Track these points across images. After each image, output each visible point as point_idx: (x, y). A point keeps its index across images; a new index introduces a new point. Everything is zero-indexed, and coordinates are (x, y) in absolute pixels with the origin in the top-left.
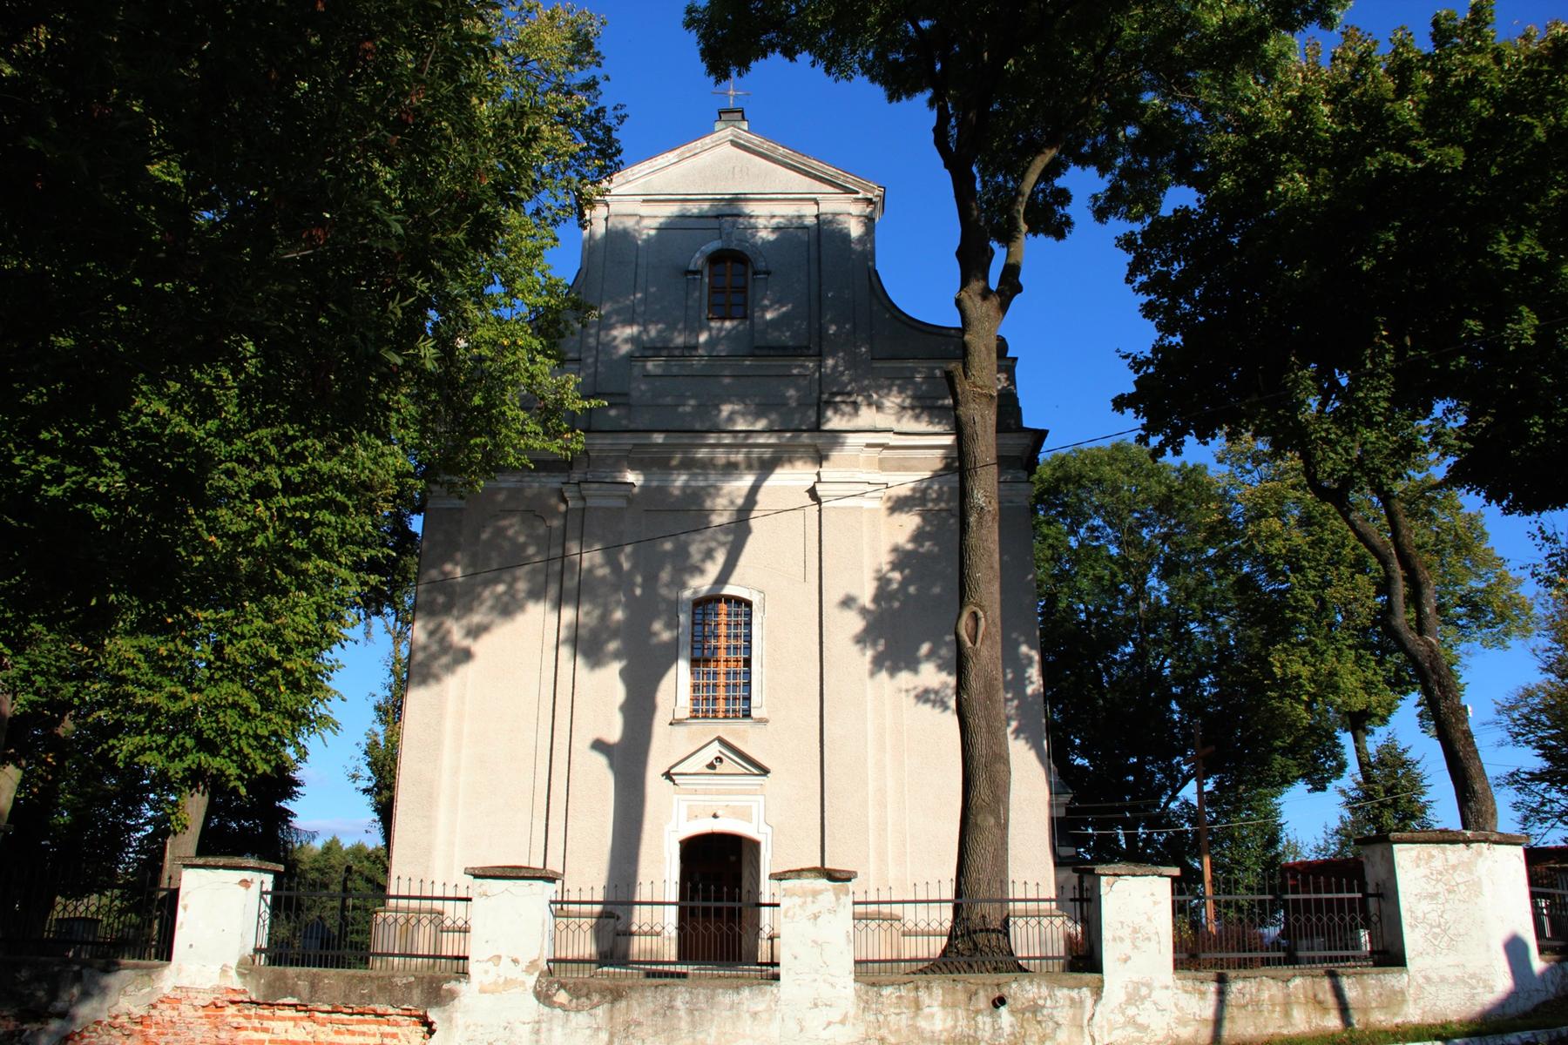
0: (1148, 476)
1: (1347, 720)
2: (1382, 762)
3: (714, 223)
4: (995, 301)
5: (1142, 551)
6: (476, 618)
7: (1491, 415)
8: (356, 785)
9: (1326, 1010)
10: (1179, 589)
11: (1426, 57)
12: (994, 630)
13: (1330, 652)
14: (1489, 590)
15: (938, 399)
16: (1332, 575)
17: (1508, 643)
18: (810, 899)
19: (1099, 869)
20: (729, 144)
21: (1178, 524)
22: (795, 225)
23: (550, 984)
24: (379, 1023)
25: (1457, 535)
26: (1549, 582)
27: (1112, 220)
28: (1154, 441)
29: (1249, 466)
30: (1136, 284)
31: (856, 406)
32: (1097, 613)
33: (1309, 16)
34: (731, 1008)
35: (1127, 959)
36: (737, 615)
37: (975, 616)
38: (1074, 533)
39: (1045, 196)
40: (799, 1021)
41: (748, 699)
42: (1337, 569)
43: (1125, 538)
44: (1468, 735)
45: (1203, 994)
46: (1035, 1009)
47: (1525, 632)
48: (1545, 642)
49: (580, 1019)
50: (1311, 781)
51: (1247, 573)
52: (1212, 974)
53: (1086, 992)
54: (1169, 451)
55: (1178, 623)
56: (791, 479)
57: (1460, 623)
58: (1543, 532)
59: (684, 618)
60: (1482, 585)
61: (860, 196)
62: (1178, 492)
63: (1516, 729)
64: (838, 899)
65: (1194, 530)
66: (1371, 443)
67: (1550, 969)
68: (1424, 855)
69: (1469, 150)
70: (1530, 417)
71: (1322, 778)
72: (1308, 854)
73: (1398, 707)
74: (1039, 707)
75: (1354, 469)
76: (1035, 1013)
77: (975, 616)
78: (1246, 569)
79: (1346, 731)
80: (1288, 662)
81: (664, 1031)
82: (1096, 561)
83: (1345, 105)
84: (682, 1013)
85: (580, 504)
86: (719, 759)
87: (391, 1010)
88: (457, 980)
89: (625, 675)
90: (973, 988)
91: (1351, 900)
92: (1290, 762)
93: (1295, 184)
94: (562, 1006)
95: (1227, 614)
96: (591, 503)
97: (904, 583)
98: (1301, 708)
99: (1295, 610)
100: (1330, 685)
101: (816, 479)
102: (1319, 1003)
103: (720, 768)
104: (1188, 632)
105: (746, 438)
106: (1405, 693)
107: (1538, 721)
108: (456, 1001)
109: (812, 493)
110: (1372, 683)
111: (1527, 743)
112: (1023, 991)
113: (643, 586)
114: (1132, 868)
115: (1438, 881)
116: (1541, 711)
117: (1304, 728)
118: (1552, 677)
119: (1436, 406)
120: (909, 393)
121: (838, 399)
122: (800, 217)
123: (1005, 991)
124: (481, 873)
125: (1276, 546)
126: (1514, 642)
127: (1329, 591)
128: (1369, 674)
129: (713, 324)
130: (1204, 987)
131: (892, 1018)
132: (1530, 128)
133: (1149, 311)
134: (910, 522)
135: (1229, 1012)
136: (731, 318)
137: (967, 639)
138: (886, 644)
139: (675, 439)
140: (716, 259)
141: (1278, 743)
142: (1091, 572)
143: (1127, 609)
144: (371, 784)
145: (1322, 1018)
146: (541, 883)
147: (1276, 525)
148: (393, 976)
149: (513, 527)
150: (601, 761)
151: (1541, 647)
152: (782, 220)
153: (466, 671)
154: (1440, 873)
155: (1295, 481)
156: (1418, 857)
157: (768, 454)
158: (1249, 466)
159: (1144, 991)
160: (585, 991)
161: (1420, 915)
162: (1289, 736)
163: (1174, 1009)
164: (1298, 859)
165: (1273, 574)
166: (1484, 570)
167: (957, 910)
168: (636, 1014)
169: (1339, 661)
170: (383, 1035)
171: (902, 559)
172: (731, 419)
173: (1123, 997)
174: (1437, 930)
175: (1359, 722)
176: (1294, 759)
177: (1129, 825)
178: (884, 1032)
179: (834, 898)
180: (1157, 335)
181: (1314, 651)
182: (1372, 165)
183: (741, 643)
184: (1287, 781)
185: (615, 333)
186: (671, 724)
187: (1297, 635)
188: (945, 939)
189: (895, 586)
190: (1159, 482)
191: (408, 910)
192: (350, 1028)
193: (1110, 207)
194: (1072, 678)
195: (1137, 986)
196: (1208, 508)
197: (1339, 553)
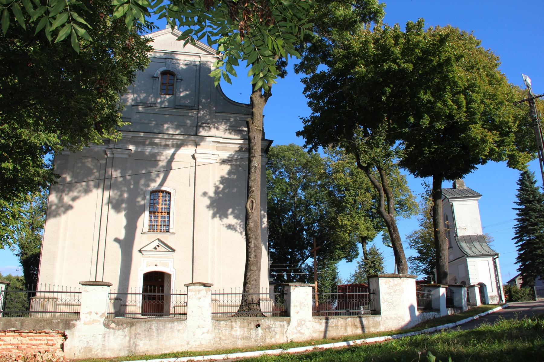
0: (300, 156)
1: (360, 239)
2: (371, 253)
3: (164, 61)
4: (264, 98)
5: (297, 181)
6: (75, 194)
7: (414, 147)
8: (13, 253)
9: (357, 328)
10: (308, 194)
11: (404, 34)
12: (258, 207)
13: (357, 217)
14: (406, 200)
15: (238, 127)
16: (359, 192)
17: (411, 217)
18: (198, 292)
19: (290, 284)
20: (170, 33)
21: (309, 173)
22: (193, 64)
23: (109, 321)
24: (47, 336)
25: (398, 182)
26: (426, 199)
27: (300, 73)
28: (309, 147)
29: (334, 155)
30: (306, 95)
31: (210, 128)
32: (280, 201)
33: (371, 19)
34: (171, 328)
35: (298, 312)
36: (165, 197)
37: (252, 202)
38: (274, 173)
39: (279, 63)
40: (193, 333)
41: (168, 226)
42: (360, 190)
43: (291, 176)
44: (401, 245)
45: (321, 323)
46: (269, 328)
47: (416, 213)
48: (421, 217)
49: (120, 333)
50: (348, 259)
51: (331, 191)
52: (324, 317)
53: (285, 323)
54: (313, 151)
55: (307, 205)
56: (186, 151)
57: (397, 210)
58: (425, 184)
59: (148, 197)
60: (404, 198)
61: (215, 56)
62: (310, 162)
63: (411, 244)
64: (207, 293)
65: (314, 175)
66: (378, 153)
67: (420, 315)
68: (388, 281)
69: (414, 65)
70: (424, 148)
71: (351, 258)
72: (344, 283)
73: (377, 235)
74: (266, 231)
75: (372, 161)
76: (269, 329)
77: (252, 202)
78: (331, 189)
79: (359, 243)
80: (343, 220)
81: (148, 336)
82: (281, 183)
83: (378, 45)
84: (154, 330)
85: (112, 156)
86: (158, 246)
87: (51, 331)
88: (76, 320)
89: (126, 216)
90: (250, 321)
91: (366, 295)
92: (341, 252)
93: (361, 69)
94: (113, 329)
95: (323, 203)
96: (116, 155)
97: (223, 189)
98: (347, 235)
99: (346, 203)
100: (356, 227)
101: (195, 152)
102: (355, 326)
103: (158, 249)
104: (310, 209)
105: (172, 136)
106: (379, 231)
107: (418, 241)
108: (75, 327)
109: (193, 157)
110: (369, 228)
111: (414, 248)
112: (266, 322)
113: (134, 185)
114: (300, 284)
115: (391, 289)
116: (419, 238)
117: (347, 241)
118: (423, 227)
119: (396, 142)
120: (228, 124)
121: (204, 125)
122: (195, 61)
123: (260, 322)
124: (85, 283)
125: (341, 182)
126: (412, 216)
127: (357, 198)
128: (368, 225)
129: (162, 96)
130: (321, 321)
131: (224, 331)
132: (432, 60)
133: (310, 104)
134: (226, 168)
135: (329, 328)
136: (168, 94)
137: (249, 209)
138: (217, 210)
139: (147, 135)
140: (164, 73)
141: (338, 246)
142: (280, 187)
143: (290, 200)
144: (19, 253)
145: (356, 330)
146: (106, 287)
147: (342, 175)
148: (52, 320)
149: (89, 163)
150: (117, 245)
151: (420, 218)
152: (189, 62)
153: (70, 212)
154: (392, 287)
155: (349, 161)
156: (386, 282)
157: (179, 142)
158: (334, 155)
159: (303, 322)
160: (121, 323)
161: (385, 299)
162: (342, 243)
163: (312, 328)
164: (341, 284)
165: (340, 191)
166: (405, 193)
167: (244, 297)
168: (139, 331)
169: (359, 220)
170: (48, 340)
171: (223, 180)
172: (168, 129)
173: (296, 324)
174: (390, 304)
175: (364, 240)
176: (343, 251)
177: (287, 272)
178: (221, 336)
179: (205, 292)
180: (312, 112)
181: (352, 217)
182: (386, 67)
183: (167, 206)
184: (340, 258)
185: (128, 96)
186: (142, 233)
187: (346, 211)
188: (239, 308)
189: (220, 189)
190: (304, 158)
191: (44, 298)
192: (35, 338)
193: (300, 69)
194: (272, 222)
195: (301, 320)
196: (320, 168)
197: (361, 185)
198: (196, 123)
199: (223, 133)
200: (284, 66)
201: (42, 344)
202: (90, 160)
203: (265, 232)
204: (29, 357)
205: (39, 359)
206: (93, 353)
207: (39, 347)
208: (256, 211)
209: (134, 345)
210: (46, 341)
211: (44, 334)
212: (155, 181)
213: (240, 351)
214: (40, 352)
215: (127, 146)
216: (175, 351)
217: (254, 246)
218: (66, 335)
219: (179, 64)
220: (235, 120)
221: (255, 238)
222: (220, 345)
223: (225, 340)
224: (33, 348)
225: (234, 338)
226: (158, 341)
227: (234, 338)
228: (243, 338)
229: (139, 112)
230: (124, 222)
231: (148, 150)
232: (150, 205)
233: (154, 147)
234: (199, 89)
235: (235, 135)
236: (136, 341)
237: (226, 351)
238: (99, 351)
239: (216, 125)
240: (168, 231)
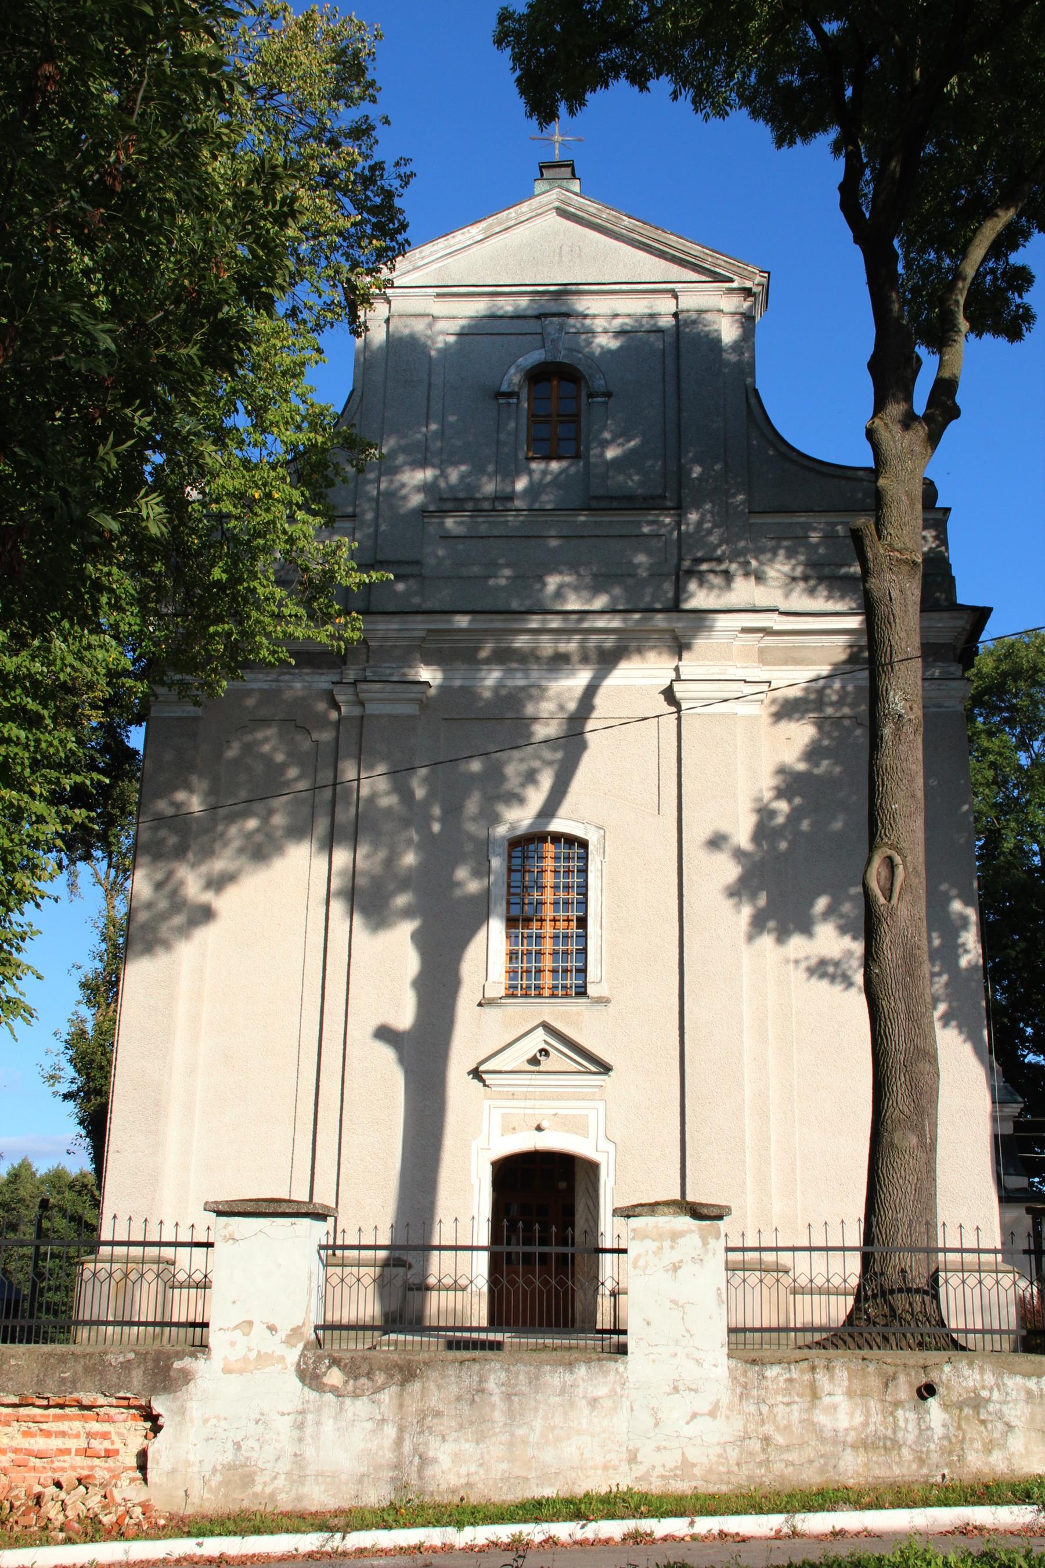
3: (533, 326)
6: (219, 865)
8: (54, 1089)
15: (842, 566)
18: (667, 1244)
20: (553, 214)
22: (646, 327)
24: (86, 1419)
31: (728, 576)
36: (568, 858)
39: (995, 279)
40: (654, 1412)
41: (583, 971)
46: (977, 1403)
49: (359, 1408)
59: (497, 863)
61: (735, 285)
64: (705, 1244)
81: (471, 1423)
84: (496, 1399)
85: (357, 711)
86: (544, 1052)
87: (101, 1400)
88: (193, 1355)
89: (419, 939)
90: (891, 1370)
94: (334, 1390)
97: (794, 817)
101: (673, 675)
103: (546, 1064)
105: (580, 621)
108: (192, 1384)
109: (669, 695)
113: (443, 820)
120: (802, 558)
121: (704, 567)
122: (652, 316)
123: (934, 1376)
129: (534, 465)
131: (780, 1409)
136: (559, 458)
137: (879, 893)
139: (484, 623)
140: (537, 375)
144: (74, 1087)
146: (307, 1221)
148: (105, 1353)
150: (387, 1054)
152: (627, 320)
153: (206, 935)
157: (610, 642)
160: (365, 1368)
167: (867, 1260)
168: (434, 1400)
170: (90, 1435)
172: (559, 594)
178: (769, 1429)
183: (573, 896)
186: (480, 1005)
188: (851, 1300)
189: (780, 820)
192: (44, 1426)
198: (675, 561)
199: (779, 593)
200: (1020, 291)
201: (67, 1452)
202: (271, 732)
203: (973, 985)
204: (17, 1503)
205: (52, 1515)
206: (258, 1488)
207: (56, 1464)
208: (908, 898)
209: (417, 1459)
210: (83, 1436)
211: (75, 1411)
212: (521, 800)
213: (847, 1501)
214: (58, 1485)
215: (412, 672)
216: (580, 1491)
217: (903, 1047)
218: (158, 1416)
219: (592, 332)
220: (829, 537)
221: (908, 1011)
222: (768, 1468)
223: (788, 1448)
224: (34, 1468)
225: (823, 1440)
226: (511, 1445)
227: (823, 1440)
228: (865, 1445)
229: (447, 537)
230: (411, 963)
231: (491, 678)
232: (509, 894)
233: (515, 665)
234: (679, 426)
235: (828, 598)
236: (426, 1444)
237: (791, 1496)
238: (281, 1482)
239: (754, 563)
240: (582, 992)
